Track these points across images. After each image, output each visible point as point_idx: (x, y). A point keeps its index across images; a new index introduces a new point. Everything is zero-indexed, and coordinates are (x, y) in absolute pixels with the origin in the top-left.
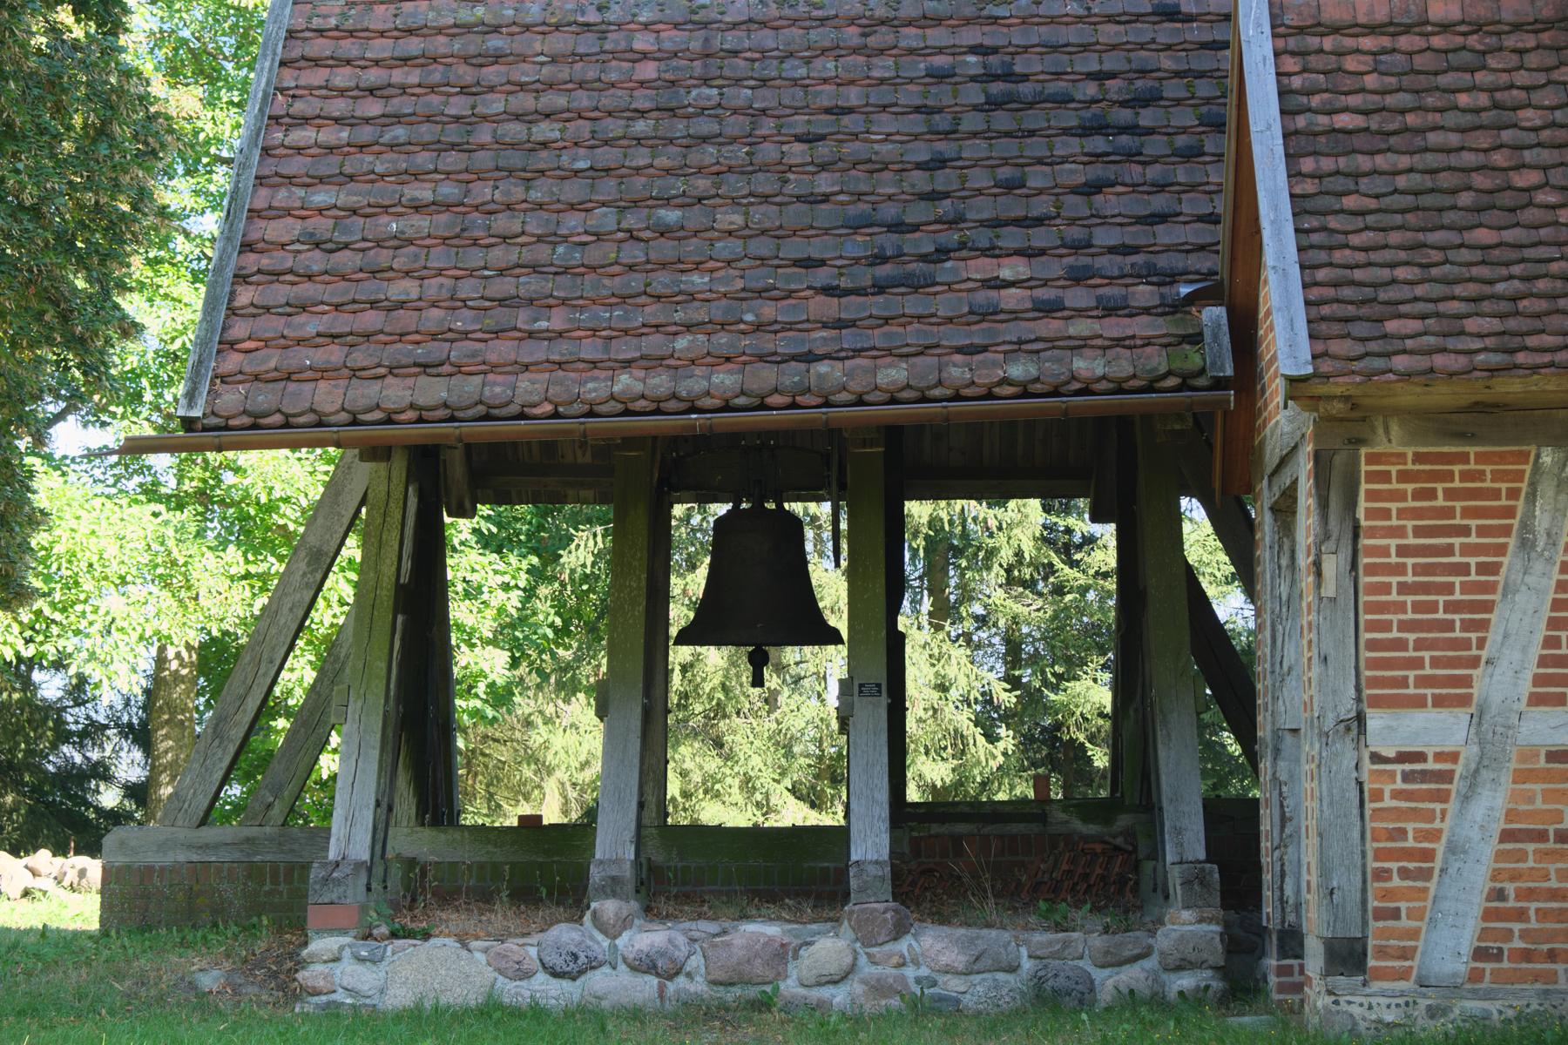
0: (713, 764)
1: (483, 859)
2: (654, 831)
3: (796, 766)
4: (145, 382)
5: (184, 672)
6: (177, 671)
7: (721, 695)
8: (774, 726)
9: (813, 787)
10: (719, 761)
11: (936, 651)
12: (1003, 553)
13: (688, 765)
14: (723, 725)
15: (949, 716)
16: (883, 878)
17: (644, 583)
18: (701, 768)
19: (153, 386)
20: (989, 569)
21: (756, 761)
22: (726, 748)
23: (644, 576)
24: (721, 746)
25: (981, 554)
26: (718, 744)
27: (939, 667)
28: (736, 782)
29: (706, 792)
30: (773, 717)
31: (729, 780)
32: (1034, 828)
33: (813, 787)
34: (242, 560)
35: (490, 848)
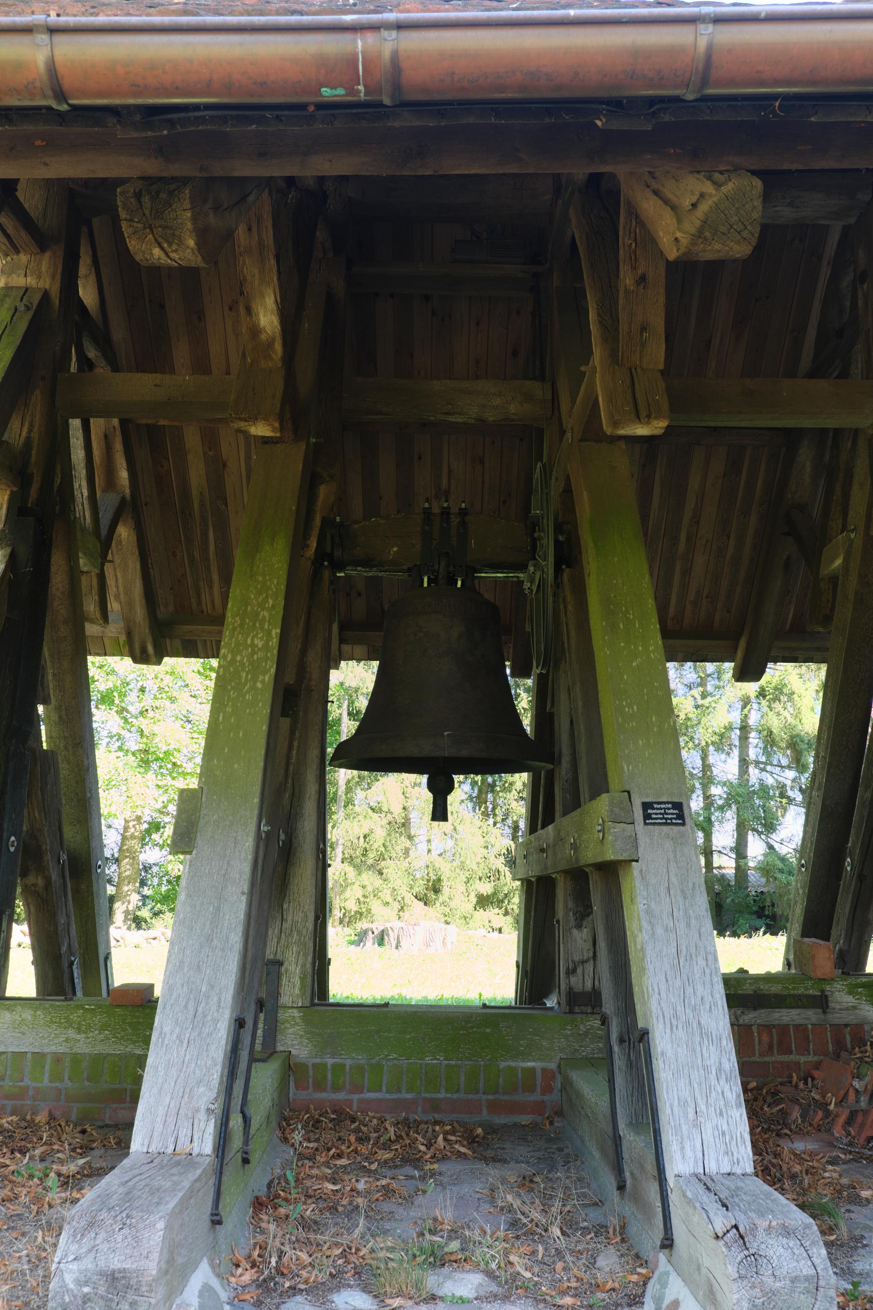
0: (377, 882)
1: (61, 1049)
2: (296, 1013)
3: (417, 884)
4: (115, 694)
5: (136, 834)
6: (133, 833)
7: (383, 849)
8: (408, 865)
9: (426, 895)
10: (381, 882)
11: (485, 831)
12: (517, 784)
13: (366, 883)
14: (383, 864)
15: (492, 862)
16: (815, 1285)
17: (275, 642)
18: (372, 884)
19: (120, 696)
20: (510, 791)
21: (399, 882)
22: (384, 875)
23: (276, 632)
24: (382, 874)
25: (507, 785)
26: (381, 873)
27: (486, 837)
28: (389, 892)
29: (374, 896)
30: (407, 860)
31: (385, 891)
32: (811, 1016)
33: (426, 895)
34: (154, 778)
35: (71, 1034)
